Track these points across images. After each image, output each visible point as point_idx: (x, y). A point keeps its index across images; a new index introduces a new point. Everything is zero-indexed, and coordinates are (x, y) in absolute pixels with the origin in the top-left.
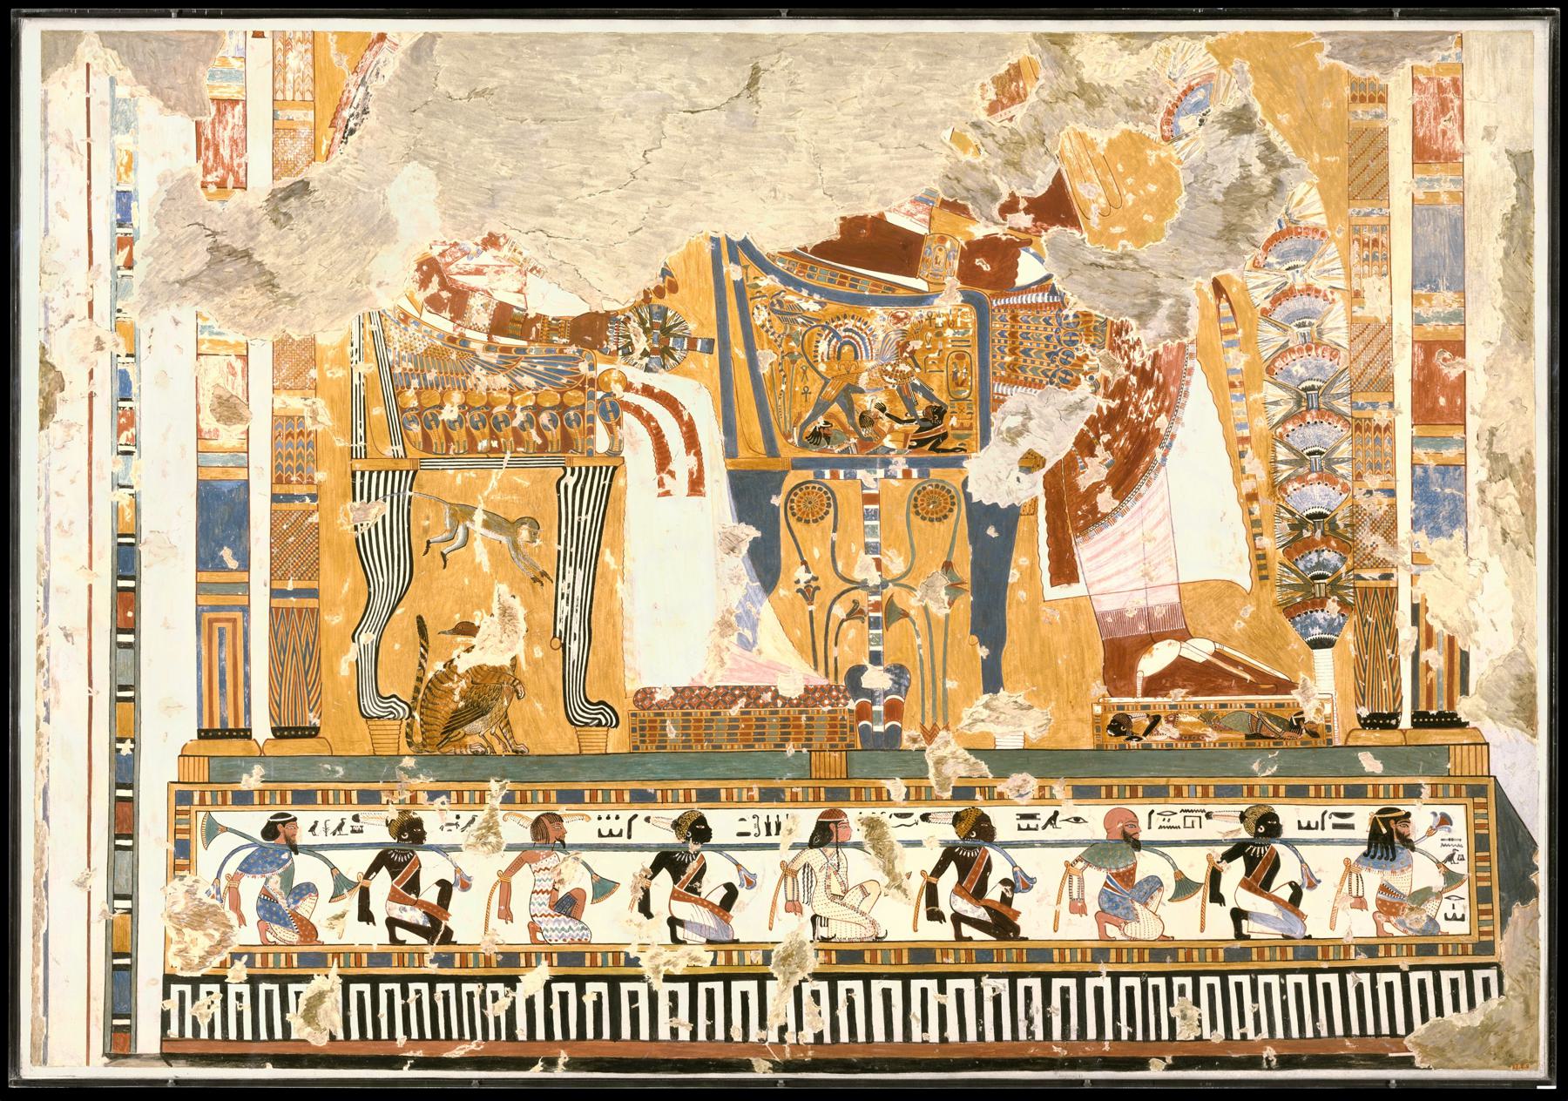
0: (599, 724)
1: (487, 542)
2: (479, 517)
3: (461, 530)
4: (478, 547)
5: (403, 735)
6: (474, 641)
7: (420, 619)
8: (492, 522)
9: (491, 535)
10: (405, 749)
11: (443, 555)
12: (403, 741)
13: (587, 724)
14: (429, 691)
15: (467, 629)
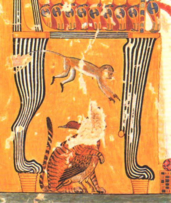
2: (82, 64)
5: (38, 182)
7: (48, 119)
9: (88, 74)
10: (39, 189)
13: (137, 178)
14: (52, 158)
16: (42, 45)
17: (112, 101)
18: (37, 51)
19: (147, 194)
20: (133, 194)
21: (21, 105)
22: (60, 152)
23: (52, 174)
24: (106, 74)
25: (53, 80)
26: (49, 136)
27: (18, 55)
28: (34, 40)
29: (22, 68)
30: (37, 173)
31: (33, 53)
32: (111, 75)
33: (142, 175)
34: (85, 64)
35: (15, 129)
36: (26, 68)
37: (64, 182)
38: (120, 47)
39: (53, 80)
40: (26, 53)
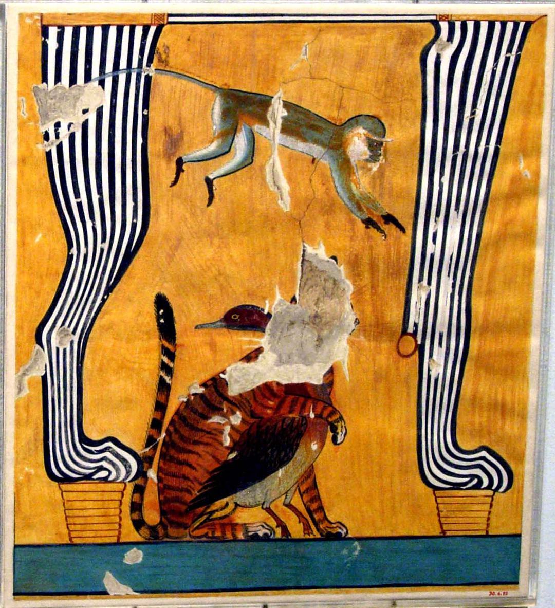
0: (478, 486)
1: (291, 161)
2: (278, 112)
3: (241, 142)
4: (275, 165)
5: (126, 508)
6: (263, 341)
7: (161, 302)
8: (300, 123)
9: (290, 141)
10: (130, 533)
11: (209, 182)
12: (128, 523)
13: (457, 486)
14: (177, 430)
15: (247, 318)
16: (474, 106)
17: (373, 231)
18: (136, 70)
19: (487, 536)
20: (443, 535)
21: (70, 258)
22: (205, 413)
23: (174, 482)
24: (357, 146)
25: (179, 170)
26: (166, 360)
27: (59, 84)
28: (126, 30)
29: (72, 130)
30: (123, 482)
31: (109, 82)
32: (375, 147)
33: (473, 477)
34: (285, 114)
35: (49, 341)
36: (85, 126)
37: (213, 508)
38: (223, 29)
39: (179, 170)
40: (88, 78)
